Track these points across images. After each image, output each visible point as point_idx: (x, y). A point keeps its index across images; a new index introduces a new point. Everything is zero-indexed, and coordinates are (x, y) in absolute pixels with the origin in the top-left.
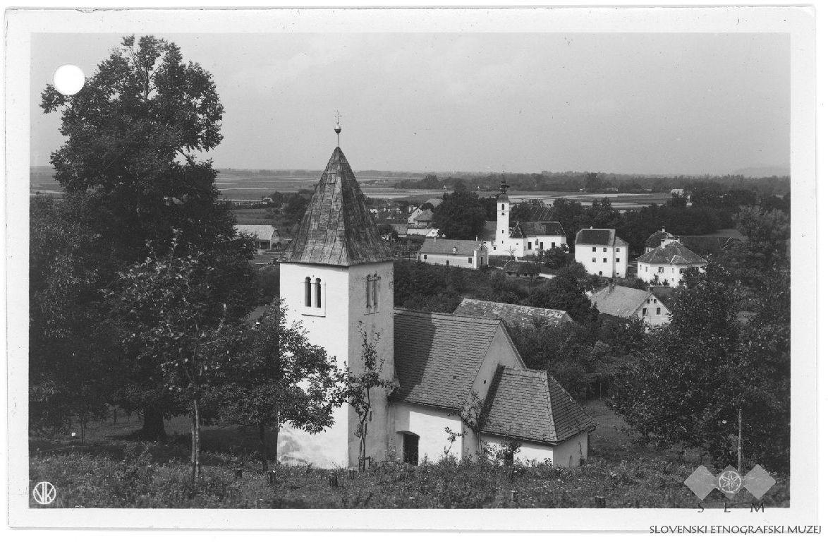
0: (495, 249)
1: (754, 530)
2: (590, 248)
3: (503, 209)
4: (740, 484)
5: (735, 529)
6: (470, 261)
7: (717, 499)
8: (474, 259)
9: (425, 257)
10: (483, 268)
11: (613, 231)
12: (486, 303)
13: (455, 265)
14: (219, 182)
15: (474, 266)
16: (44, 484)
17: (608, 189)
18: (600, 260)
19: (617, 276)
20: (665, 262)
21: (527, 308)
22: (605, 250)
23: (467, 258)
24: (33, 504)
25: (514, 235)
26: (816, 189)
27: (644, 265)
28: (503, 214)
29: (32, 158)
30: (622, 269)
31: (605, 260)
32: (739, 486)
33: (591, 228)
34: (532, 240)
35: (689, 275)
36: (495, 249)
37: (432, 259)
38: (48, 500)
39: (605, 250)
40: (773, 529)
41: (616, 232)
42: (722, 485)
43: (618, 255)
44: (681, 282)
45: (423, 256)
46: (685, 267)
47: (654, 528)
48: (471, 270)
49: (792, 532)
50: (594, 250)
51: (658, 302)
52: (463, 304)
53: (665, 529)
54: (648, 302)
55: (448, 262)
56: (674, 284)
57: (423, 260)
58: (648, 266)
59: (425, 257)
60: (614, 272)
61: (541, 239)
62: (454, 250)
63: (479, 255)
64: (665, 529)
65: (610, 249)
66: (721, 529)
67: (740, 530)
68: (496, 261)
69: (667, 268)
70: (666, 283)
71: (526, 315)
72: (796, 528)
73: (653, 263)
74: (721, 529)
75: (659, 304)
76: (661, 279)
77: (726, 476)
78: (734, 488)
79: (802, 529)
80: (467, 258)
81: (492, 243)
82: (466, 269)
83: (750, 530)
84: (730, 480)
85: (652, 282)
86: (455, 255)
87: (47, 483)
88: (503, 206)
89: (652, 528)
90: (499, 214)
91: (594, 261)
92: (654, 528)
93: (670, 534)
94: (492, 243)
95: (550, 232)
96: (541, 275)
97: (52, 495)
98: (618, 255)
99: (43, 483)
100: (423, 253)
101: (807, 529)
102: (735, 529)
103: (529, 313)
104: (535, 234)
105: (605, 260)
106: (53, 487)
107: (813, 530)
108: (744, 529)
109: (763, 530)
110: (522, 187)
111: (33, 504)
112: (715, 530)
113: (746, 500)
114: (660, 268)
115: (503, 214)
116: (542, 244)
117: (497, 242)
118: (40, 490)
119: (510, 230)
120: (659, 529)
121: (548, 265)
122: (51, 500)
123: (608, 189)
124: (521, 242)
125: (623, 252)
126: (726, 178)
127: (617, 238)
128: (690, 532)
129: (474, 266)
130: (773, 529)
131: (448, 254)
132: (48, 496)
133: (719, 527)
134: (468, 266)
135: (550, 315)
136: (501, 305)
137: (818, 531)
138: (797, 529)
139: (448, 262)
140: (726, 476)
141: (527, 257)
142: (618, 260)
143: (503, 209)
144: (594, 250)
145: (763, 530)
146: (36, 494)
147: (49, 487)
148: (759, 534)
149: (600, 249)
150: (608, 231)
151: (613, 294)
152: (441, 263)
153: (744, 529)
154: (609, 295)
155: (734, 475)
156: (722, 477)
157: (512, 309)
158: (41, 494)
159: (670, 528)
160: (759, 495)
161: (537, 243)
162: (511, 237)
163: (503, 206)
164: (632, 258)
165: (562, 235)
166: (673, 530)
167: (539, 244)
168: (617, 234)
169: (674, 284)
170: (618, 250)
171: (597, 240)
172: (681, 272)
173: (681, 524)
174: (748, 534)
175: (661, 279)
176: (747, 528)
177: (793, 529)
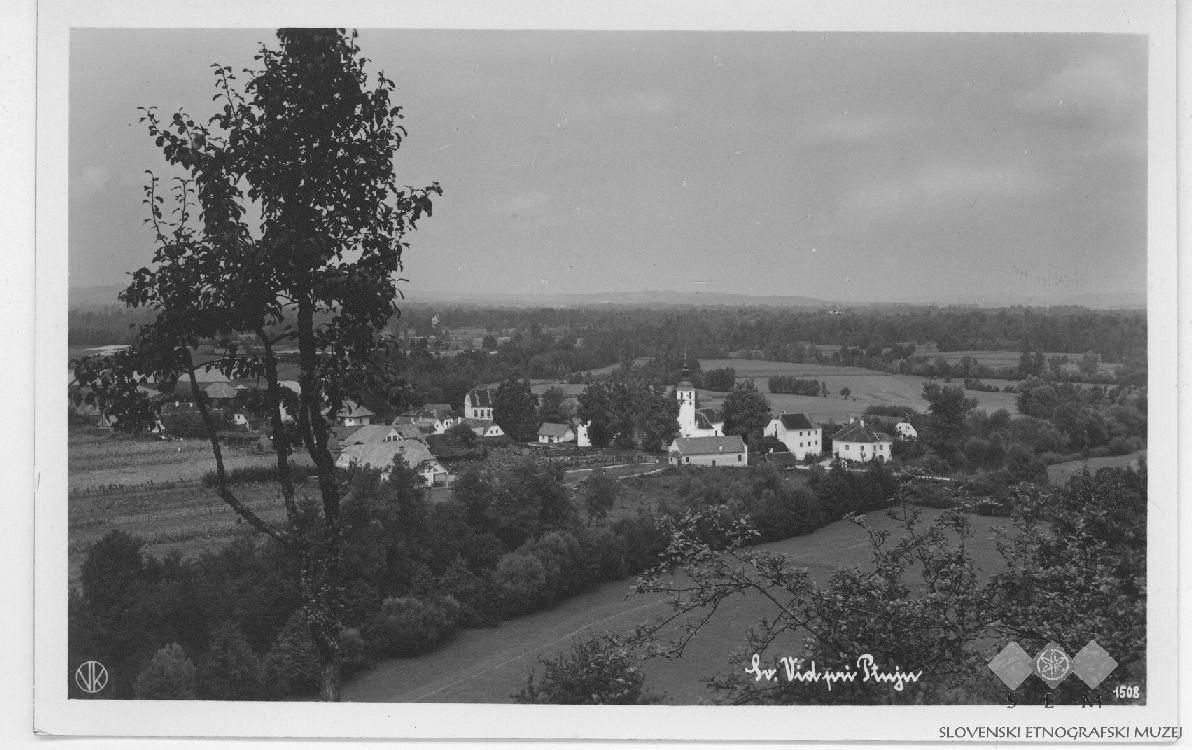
1: (1087, 733)
4: (1068, 668)
6: (740, 458)
7: (1034, 692)
8: (745, 456)
9: (687, 460)
14: (397, 301)
16: (91, 664)
23: (736, 456)
24: (76, 692)
26: (1178, 649)
32: (1065, 671)
38: (98, 687)
40: (1114, 731)
42: (1042, 669)
49: (1142, 736)
55: (714, 462)
72: (1147, 729)
77: (1048, 655)
78: (1059, 673)
79: (1155, 733)
80: (736, 456)
84: (1053, 664)
86: (721, 453)
92: (945, 731)
97: (102, 680)
99: (89, 662)
108: (1073, 733)
111: (76, 692)
113: (1074, 692)
118: (85, 670)
126: (1054, 309)
130: (1114, 731)
131: (714, 454)
134: (739, 464)
139: (714, 462)
140: (1048, 655)
147: (98, 669)
149: (805, 433)
153: (1073, 733)
155: (1059, 656)
156: (1042, 656)
158: (87, 678)
159: (968, 729)
160: (1093, 682)
176: (1078, 729)
177: (1142, 731)
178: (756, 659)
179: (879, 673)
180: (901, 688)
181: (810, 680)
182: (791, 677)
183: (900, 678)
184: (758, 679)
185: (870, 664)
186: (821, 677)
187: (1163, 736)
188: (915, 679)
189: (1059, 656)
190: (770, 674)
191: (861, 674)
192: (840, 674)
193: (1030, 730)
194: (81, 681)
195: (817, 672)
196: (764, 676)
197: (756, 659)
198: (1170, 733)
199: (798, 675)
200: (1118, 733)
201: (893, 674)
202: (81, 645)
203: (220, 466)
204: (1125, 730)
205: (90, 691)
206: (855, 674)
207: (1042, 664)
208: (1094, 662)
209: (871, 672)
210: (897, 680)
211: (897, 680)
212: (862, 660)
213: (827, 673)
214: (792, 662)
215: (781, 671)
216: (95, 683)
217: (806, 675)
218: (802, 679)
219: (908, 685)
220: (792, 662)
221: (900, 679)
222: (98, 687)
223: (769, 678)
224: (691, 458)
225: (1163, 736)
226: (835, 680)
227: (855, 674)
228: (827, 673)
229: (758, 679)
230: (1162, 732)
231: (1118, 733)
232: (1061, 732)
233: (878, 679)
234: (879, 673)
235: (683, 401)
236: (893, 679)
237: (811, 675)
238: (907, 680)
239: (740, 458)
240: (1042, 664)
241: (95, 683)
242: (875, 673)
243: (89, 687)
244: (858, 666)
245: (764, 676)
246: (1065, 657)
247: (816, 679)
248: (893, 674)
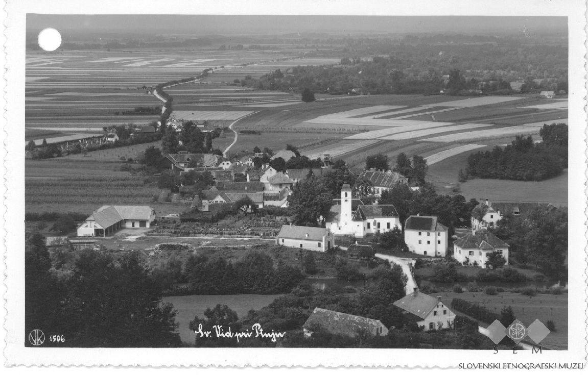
0: (340, 229)
1: (534, 366)
5: (521, 366)
6: (319, 245)
8: (323, 244)
9: (283, 241)
10: (331, 251)
11: (435, 218)
12: (330, 312)
15: (323, 249)
16: (37, 331)
17: (471, 91)
18: (424, 242)
19: (438, 255)
20: (475, 247)
21: (356, 317)
22: (429, 234)
23: (316, 243)
24: (28, 344)
25: (356, 219)
27: (459, 249)
28: (346, 201)
30: (442, 249)
31: (429, 242)
33: (418, 215)
35: (494, 259)
36: (340, 229)
37: (289, 242)
39: (429, 234)
40: (548, 365)
41: (438, 219)
42: (511, 334)
43: (439, 238)
45: (281, 240)
46: (490, 252)
47: (462, 365)
49: (562, 368)
50: (420, 234)
51: (444, 306)
52: (315, 311)
54: (438, 307)
55: (301, 245)
57: (281, 243)
59: (283, 241)
60: (436, 252)
61: (378, 220)
62: (307, 235)
63: (328, 240)
64: (470, 366)
65: (432, 234)
66: (511, 365)
67: (524, 366)
68: (342, 240)
69: (476, 252)
70: (475, 264)
71: (355, 322)
72: (565, 365)
73: (465, 248)
75: (445, 307)
76: (472, 261)
79: (569, 366)
80: (316, 243)
81: (338, 224)
85: (464, 263)
88: (346, 194)
89: (461, 365)
90: (343, 200)
92: (462, 365)
95: (386, 213)
96: (377, 255)
98: (439, 238)
100: (281, 237)
101: (573, 365)
103: (357, 321)
104: (373, 215)
105: (429, 242)
108: (527, 366)
110: (375, 90)
111: (28, 344)
112: (507, 366)
114: (470, 252)
115: (346, 201)
116: (379, 224)
117: (342, 224)
118: (33, 334)
119: (353, 213)
120: (465, 366)
121: (382, 246)
122: (42, 343)
123: (471, 91)
125: (443, 236)
127: (438, 224)
128: (488, 368)
129: (323, 249)
130: (548, 365)
132: (40, 340)
133: (509, 364)
134: (318, 249)
135: (370, 323)
136: (339, 314)
138: (566, 366)
139: (301, 245)
141: (368, 235)
142: (439, 242)
143: (346, 196)
144: (420, 234)
146: (30, 336)
147: (40, 334)
149: (424, 234)
151: (417, 298)
152: (296, 247)
154: (414, 299)
155: (520, 327)
156: (511, 327)
161: (374, 224)
162: (353, 220)
163: (346, 194)
164: (451, 242)
165: (395, 215)
166: (476, 366)
168: (438, 221)
170: (439, 234)
171: (422, 226)
172: (487, 255)
175: (472, 261)
176: (530, 365)
177: (562, 365)
178: (201, 327)
179: (263, 333)
180: (275, 341)
181: (228, 336)
182: (218, 335)
183: (274, 335)
184: (201, 336)
185: (259, 329)
186: (234, 335)
189: (520, 327)
190: (208, 334)
191: (255, 333)
192: (243, 334)
196: (205, 335)
197: (201, 327)
199: (222, 334)
200: (494, 366)
201: (271, 334)
202: (32, 322)
203: (450, 252)
204: (554, 365)
206: (251, 333)
207: (511, 332)
208: (538, 330)
209: (259, 332)
210: (272, 336)
211: (272, 336)
212: (255, 328)
213: (237, 333)
214: (219, 328)
215: (214, 333)
216: (38, 341)
217: (226, 334)
218: (224, 336)
219: (280, 339)
220: (219, 328)
221: (275, 336)
223: (207, 336)
224: (285, 240)
226: (241, 336)
227: (251, 333)
228: (237, 333)
229: (201, 336)
231: (494, 366)
232: (521, 366)
233: (263, 336)
234: (263, 333)
236: (271, 336)
237: (229, 335)
238: (278, 336)
240: (511, 332)
241: (38, 341)
242: (261, 333)
243: (35, 342)
244: (253, 329)
245: (205, 335)
246: (523, 328)
247: (231, 336)
248: (271, 334)
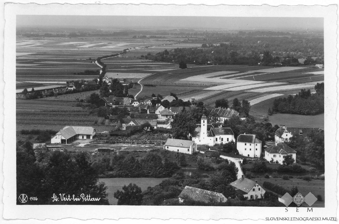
1: (309, 219)
2: (244, 144)
3: (204, 122)
6: (188, 150)
8: (190, 149)
9: (168, 148)
11: (254, 136)
13: (182, 152)
16: (23, 195)
18: (248, 149)
20: (277, 152)
23: (187, 149)
24: (19, 203)
28: (204, 125)
29: (17, 23)
32: (302, 201)
33: (245, 134)
34: (217, 137)
38: (25, 201)
40: (316, 218)
43: (256, 147)
44: (284, 162)
45: (166, 147)
46: (285, 155)
48: (188, 155)
49: (324, 220)
50: (246, 144)
53: (272, 219)
55: (178, 150)
56: (281, 163)
58: (269, 154)
59: (168, 148)
62: (181, 145)
64: (272, 219)
66: (295, 219)
67: (303, 219)
68: (201, 148)
69: (278, 155)
70: (277, 162)
72: (326, 218)
73: (271, 153)
74: (295, 219)
76: (275, 160)
78: (301, 202)
79: (328, 219)
80: (187, 149)
81: (199, 138)
82: (186, 154)
83: (307, 219)
87: (24, 194)
88: (204, 121)
89: (267, 218)
91: (245, 149)
92: (267, 218)
93: (274, 221)
94: (199, 138)
95: (227, 133)
96: (221, 156)
97: (26, 199)
98: (256, 147)
101: (330, 219)
102: (301, 219)
106: (27, 196)
107: (334, 219)
108: (304, 219)
109: (312, 219)
111: (19, 203)
114: (274, 155)
118: (21, 196)
119: (207, 132)
120: (269, 219)
121: (224, 151)
122: (26, 201)
124: (212, 138)
125: (259, 146)
127: (256, 139)
128: (282, 220)
129: (190, 153)
130: (316, 218)
133: (294, 218)
134: (188, 153)
137: (335, 219)
138: (326, 219)
139: (178, 150)
141: (216, 145)
142: (256, 149)
143: (204, 122)
144: (246, 144)
145: (312, 219)
147: (25, 196)
148: (310, 221)
149: (248, 144)
150: (252, 136)
152: (175, 151)
153: (304, 219)
156: (295, 197)
157: (203, 192)
158: (22, 199)
159: (274, 218)
161: (220, 139)
163: (204, 121)
164: (263, 149)
165: (232, 134)
166: (275, 219)
167: (221, 139)
169: (281, 163)
170: (256, 145)
173: (279, 216)
174: (306, 221)
175: (275, 160)
176: (306, 218)
177: (324, 218)
187: (331, 220)
188: (79, 200)
189: (300, 197)
193: (292, 218)
194: (20, 199)
195: (70, 198)
198: (332, 219)
205: (23, 202)
206: (80, 199)
208: (311, 198)
216: (24, 200)
222: (25, 201)
225: (331, 220)
230: (330, 219)
235: (29, 141)
239: (188, 150)
243: (22, 201)
246: (302, 197)
